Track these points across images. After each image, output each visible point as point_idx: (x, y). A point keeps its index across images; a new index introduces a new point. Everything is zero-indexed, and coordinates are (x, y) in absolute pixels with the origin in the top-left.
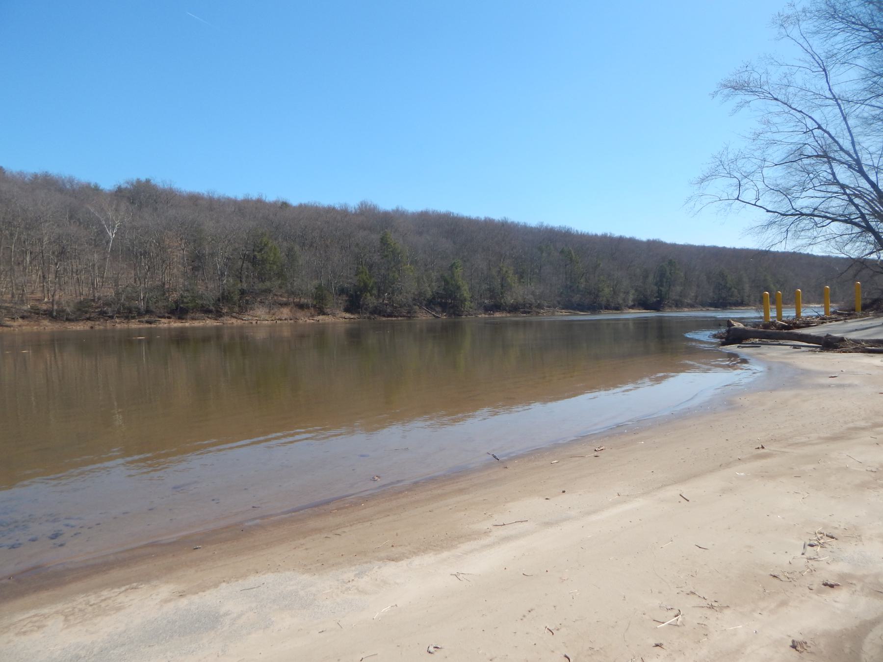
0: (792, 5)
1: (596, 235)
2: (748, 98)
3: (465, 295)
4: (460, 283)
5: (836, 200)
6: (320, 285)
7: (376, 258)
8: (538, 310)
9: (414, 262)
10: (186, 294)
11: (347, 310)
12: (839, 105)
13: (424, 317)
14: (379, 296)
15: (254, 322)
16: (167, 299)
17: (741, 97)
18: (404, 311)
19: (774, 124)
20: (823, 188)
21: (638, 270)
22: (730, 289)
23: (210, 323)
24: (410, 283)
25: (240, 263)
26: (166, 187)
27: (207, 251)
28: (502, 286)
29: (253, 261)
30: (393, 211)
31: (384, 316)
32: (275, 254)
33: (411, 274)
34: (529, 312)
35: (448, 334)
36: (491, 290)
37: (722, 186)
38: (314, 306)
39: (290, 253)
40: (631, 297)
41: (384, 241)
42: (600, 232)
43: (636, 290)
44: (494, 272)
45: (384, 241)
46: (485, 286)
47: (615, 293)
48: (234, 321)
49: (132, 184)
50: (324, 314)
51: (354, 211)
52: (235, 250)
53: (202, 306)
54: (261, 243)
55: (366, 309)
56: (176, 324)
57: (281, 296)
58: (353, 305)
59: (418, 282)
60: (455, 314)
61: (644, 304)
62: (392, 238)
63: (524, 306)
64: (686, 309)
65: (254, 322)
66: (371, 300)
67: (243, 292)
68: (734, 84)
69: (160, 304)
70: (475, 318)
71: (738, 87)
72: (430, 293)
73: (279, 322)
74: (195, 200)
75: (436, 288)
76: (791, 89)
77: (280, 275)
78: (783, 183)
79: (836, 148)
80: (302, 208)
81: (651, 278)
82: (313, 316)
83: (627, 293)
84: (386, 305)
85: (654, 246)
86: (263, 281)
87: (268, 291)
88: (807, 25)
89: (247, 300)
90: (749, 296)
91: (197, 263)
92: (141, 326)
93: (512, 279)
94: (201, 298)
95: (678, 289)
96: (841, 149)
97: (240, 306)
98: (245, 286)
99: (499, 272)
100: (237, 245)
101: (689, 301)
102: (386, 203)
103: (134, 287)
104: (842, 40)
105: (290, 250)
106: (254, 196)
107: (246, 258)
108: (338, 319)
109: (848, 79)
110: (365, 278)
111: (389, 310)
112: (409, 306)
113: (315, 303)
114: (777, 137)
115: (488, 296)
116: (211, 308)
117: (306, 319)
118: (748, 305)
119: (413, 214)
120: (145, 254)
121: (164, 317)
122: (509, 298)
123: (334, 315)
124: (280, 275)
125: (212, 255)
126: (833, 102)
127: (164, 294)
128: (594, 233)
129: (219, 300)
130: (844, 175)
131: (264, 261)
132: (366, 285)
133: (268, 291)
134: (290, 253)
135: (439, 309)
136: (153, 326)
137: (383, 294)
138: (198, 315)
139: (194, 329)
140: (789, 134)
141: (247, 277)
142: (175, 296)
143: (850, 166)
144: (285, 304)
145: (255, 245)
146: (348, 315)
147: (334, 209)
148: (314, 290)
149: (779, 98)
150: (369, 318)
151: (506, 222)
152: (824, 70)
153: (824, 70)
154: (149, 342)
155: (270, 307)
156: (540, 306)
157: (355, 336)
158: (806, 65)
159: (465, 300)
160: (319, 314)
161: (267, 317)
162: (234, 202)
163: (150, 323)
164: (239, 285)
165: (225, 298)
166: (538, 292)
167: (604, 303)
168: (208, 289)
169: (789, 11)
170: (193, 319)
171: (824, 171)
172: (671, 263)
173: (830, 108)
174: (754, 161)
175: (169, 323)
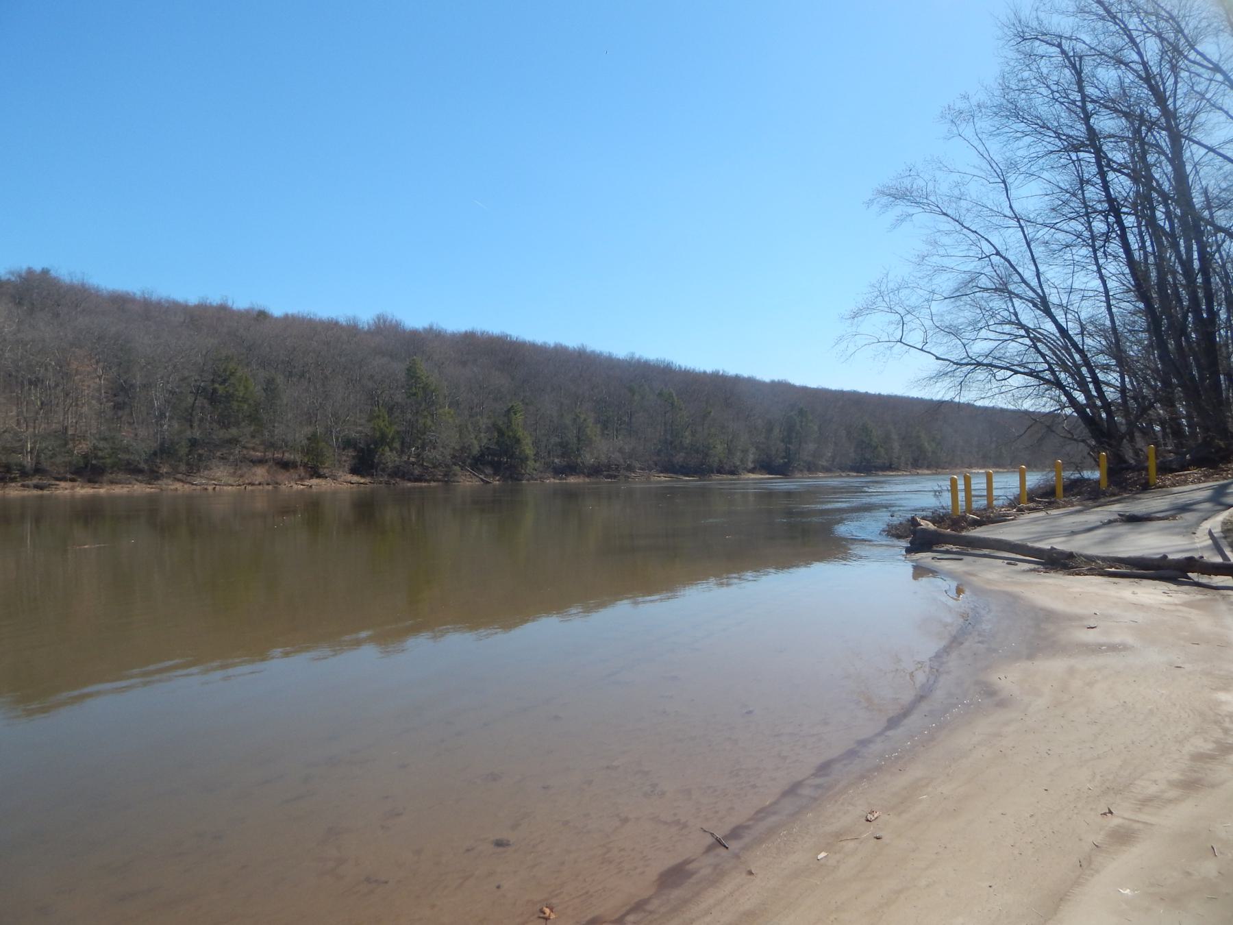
0: (966, 97)
1: (705, 373)
2: (911, 210)
3: (527, 452)
4: (519, 434)
5: (1013, 344)
6: (314, 434)
7: (399, 397)
8: (627, 474)
9: (455, 404)
10: (102, 444)
11: (354, 471)
12: (1021, 227)
13: (467, 482)
14: (402, 452)
15: (210, 488)
16: (70, 452)
17: (902, 208)
18: (439, 474)
19: (943, 246)
20: (999, 329)
21: (760, 421)
22: (876, 448)
23: (140, 489)
24: (448, 433)
25: (190, 399)
26: (75, 281)
27: (138, 380)
28: (579, 439)
29: (213, 398)
30: (425, 329)
31: (409, 480)
32: (246, 388)
33: (450, 420)
34: (615, 477)
35: (499, 508)
36: (563, 445)
37: (879, 323)
38: (305, 465)
39: (270, 387)
40: (751, 457)
41: (411, 373)
42: (709, 368)
43: (757, 448)
44: (568, 420)
45: (411, 373)
46: (555, 439)
47: (730, 451)
48: (178, 485)
49: (20, 276)
50: (319, 476)
51: (366, 327)
52: (184, 379)
53: (128, 463)
54: (225, 370)
55: (383, 470)
56: (83, 491)
57: (253, 449)
58: (364, 464)
59: (461, 432)
60: (511, 477)
61: (766, 466)
62: (423, 368)
63: (609, 467)
64: (821, 475)
65: (210, 488)
66: (390, 457)
67: (193, 443)
68: (894, 191)
69: (59, 459)
70: (540, 485)
71: (900, 195)
72: (477, 448)
73: (249, 488)
74: (120, 302)
75: (485, 441)
76: (963, 203)
77: (253, 418)
78: (948, 319)
79: (1016, 278)
80: (289, 322)
81: (776, 431)
82: (302, 479)
83: (745, 451)
84: (413, 464)
85: (781, 389)
86: (226, 427)
87: (233, 441)
88: (984, 124)
89: (200, 455)
90: (899, 458)
91: (121, 396)
92: (26, 493)
93: (593, 430)
94: (126, 450)
95: (811, 446)
96: (1024, 281)
97: (188, 464)
98: (197, 434)
99: (575, 420)
100: (187, 374)
101: (825, 464)
102: (415, 318)
103: (16, 434)
104: (1025, 147)
105: (270, 381)
106: (215, 298)
107: (199, 391)
108: (340, 485)
109: (1032, 196)
110: (382, 425)
111: (416, 472)
112: (447, 466)
113: (306, 460)
114: (947, 262)
115: (559, 452)
116: (143, 466)
117: (292, 485)
118: (897, 469)
119: (453, 335)
120: (35, 383)
121: (64, 479)
122: (588, 456)
123: (335, 478)
124: (253, 418)
125: (146, 386)
126: (1014, 223)
127: (66, 444)
128: (702, 370)
129: (155, 454)
130: (1028, 316)
131: (229, 397)
132: (383, 436)
133: (233, 441)
134: (270, 387)
135: (489, 471)
136: (46, 492)
137: (409, 448)
138: (121, 476)
139: (113, 499)
140: (961, 260)
141: (201, 420)
142: (84, 447)
143: (1035, 305)
144: (261, 462)
145: (215, 373)
146: (355, 479)
147: (336, 323)
148: (305, 442)
149: (949, 212)
150: (387, 483)
151: (584, 351)
152: (1004, 182)
153: (1004, 182)
154: (38, 520)
155: (236, 464)
156: (630, 468)
157: (365, 510)
158: (983, 174)
159: (527, 458)
160: (311, 477)
161: (231, 481)
162: (184, 309)
163: (41, 488)
164: (189, 433)
165: (165, 451)
166: (627, 449)
167: (715, 465)
168: (138, 438)
169: (961, 105)
170: (112, 482)
171: (997, 303)
172: (801, 412)
173: (1011, 230)
174: (921, 292)
175: (73, 488)
